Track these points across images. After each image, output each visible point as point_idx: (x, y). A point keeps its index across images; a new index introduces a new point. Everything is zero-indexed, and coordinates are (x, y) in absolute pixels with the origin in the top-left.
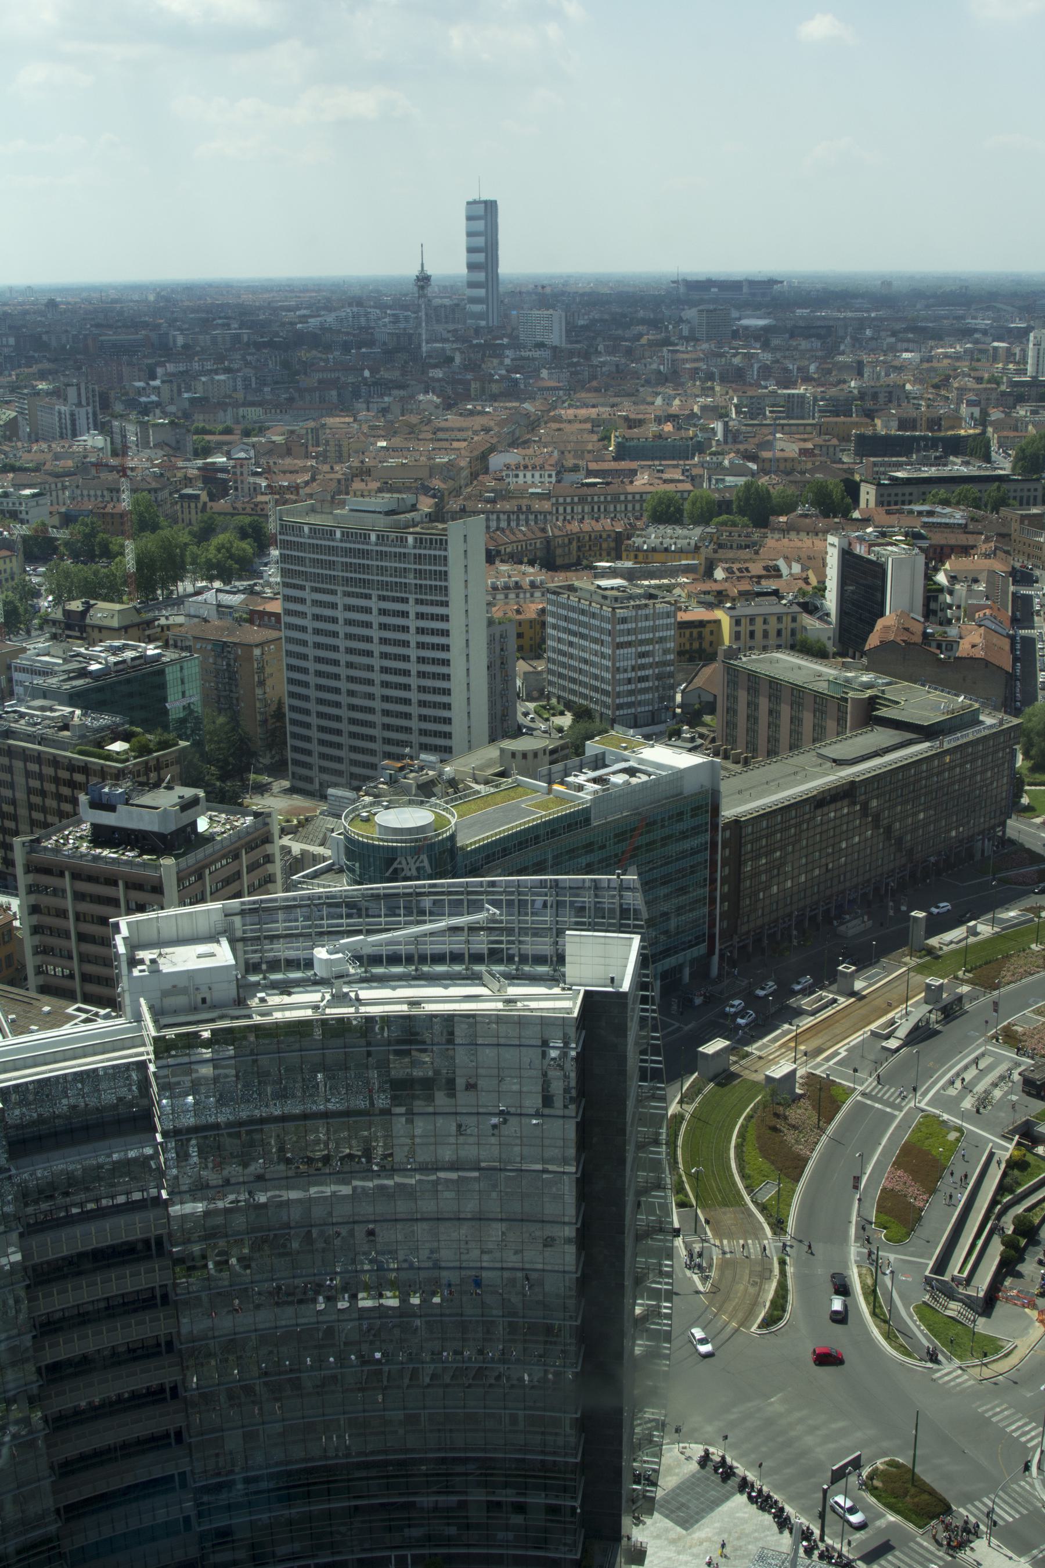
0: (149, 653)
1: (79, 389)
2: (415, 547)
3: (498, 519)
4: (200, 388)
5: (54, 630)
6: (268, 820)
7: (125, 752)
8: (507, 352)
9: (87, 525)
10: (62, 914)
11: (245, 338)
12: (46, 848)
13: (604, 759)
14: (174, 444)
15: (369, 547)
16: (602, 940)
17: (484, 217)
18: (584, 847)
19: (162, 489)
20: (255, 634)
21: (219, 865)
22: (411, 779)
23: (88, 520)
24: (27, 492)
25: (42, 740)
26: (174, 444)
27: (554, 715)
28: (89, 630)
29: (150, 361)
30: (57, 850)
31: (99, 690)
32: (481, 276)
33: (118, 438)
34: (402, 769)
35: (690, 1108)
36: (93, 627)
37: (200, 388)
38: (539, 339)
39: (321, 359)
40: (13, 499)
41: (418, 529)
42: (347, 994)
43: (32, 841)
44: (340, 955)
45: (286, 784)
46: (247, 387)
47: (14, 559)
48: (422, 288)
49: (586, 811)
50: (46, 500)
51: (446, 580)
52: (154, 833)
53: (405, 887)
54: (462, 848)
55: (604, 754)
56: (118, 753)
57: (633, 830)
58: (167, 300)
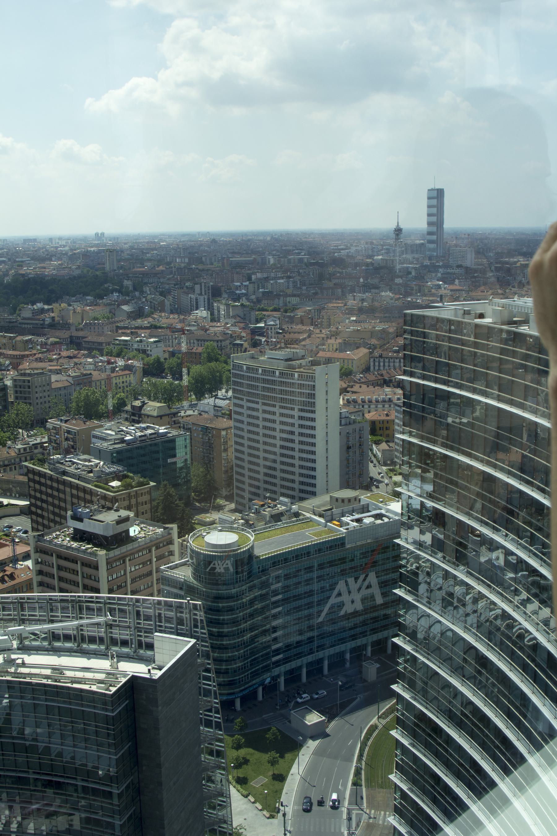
0: (160, 431)
1: (201, 286)
2: (298, 380)
3: (394, 362)
4: (270, 287)
5: (126, 416)
6: (171, 531)
7: (118, 487)
8: (440, 270)
9: (179, 358)
10: (52, 576)
11: (306, 260)
12: (45, 540)
13: (368, 507)
14: (242, 316)
15: (275, 379)
16: (174, 641)
17: (437, 198)
18: (339, 560)
19: (224, 340)
20: (224, 423)
21: (140, 554)
22: (267, 512)
23: (180, 356)
24: (152, 340)
25: (79, 478)
26: (242, 316)
27: (395, 475)
28: (143, 416)
29: (249, 272)
30: (50, 542)
31: (127, 451)
32: (434, 229)
33: (216, 312)
34: (263, 506)
35: (384, 722)
36: (145, 415)
37: (270, 287)
38: (460, 263)
39: (339, 272)
40: (144, 343)
41: (302, 370)
42: (14, 660)
43: (39, 535)
44: (7, 637)
45: (233, 506)
46: (295, 287)
47: (132, 375)
48: (397, 235)
49: (343, 538)
50: (161, 344)
51: (314, 399)
52: (102, 536)
53: (71, 596)
54: (258, 557)
55: (368, 505)
56: (113, 487)
57: (373, 551)
58: (276, 240)
